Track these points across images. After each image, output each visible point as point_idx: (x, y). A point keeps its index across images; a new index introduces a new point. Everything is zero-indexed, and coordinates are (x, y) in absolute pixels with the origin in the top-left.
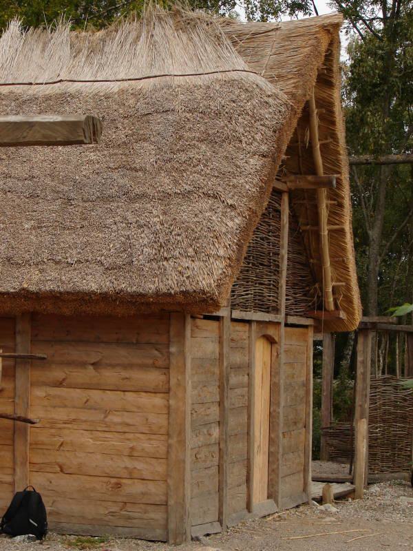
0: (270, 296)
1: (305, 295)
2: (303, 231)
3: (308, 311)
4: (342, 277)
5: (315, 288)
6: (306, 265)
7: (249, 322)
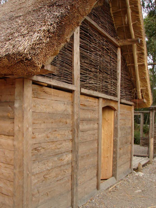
0: (112, 89)
1: (130, 93)
2: (128, 66)
3: (131, 99)
4: (144, 85)
5: (134, 90)
6: (130, 80)
7: (98, 98)
